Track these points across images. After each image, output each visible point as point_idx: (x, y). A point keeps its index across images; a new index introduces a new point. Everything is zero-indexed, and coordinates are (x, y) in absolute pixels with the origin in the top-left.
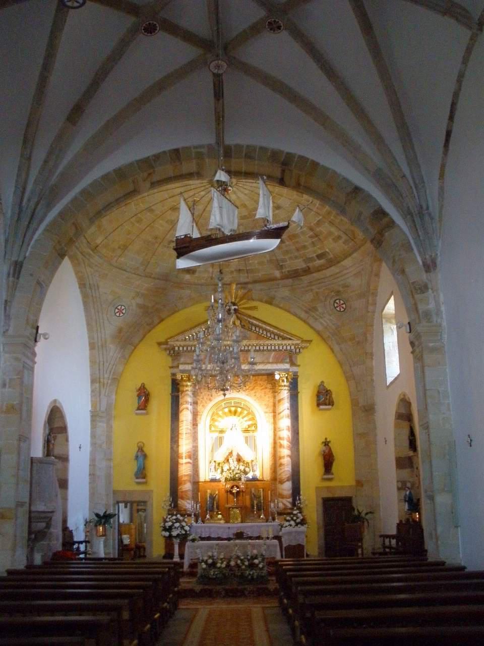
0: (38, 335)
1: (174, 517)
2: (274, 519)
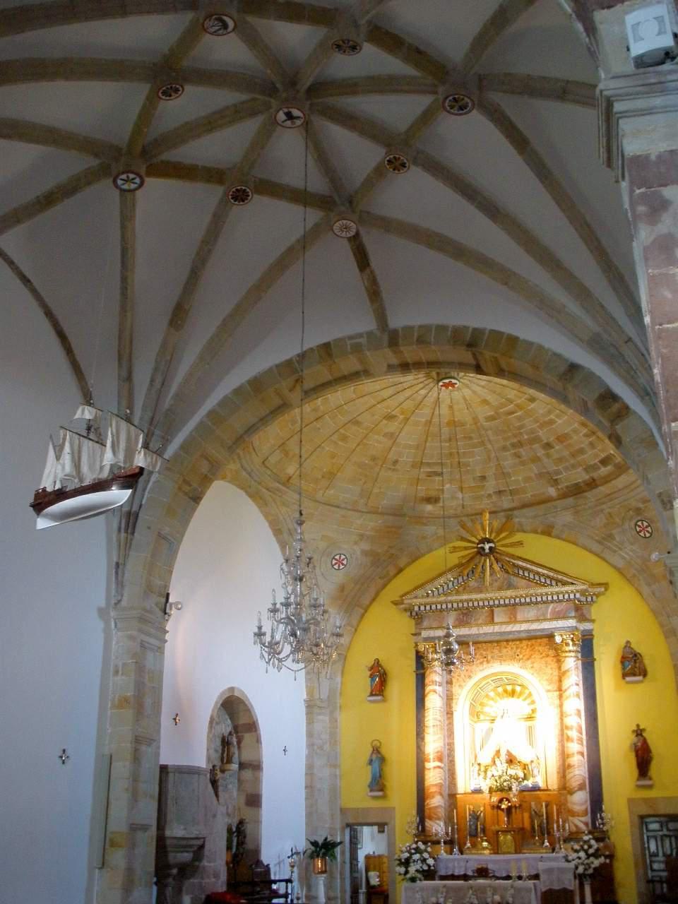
0: (168, 605)
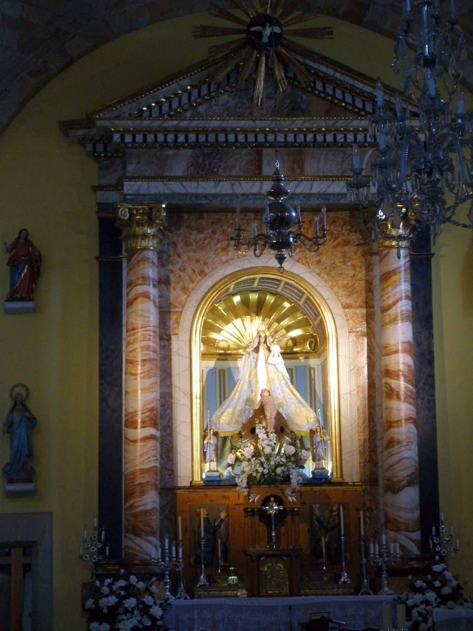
1: (122, 583)
2: (375, 588)
